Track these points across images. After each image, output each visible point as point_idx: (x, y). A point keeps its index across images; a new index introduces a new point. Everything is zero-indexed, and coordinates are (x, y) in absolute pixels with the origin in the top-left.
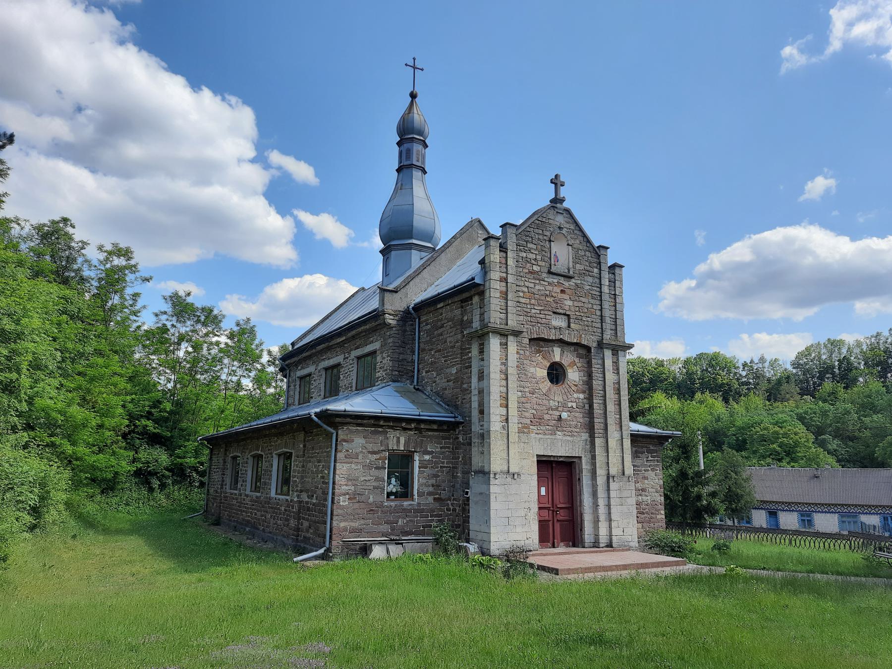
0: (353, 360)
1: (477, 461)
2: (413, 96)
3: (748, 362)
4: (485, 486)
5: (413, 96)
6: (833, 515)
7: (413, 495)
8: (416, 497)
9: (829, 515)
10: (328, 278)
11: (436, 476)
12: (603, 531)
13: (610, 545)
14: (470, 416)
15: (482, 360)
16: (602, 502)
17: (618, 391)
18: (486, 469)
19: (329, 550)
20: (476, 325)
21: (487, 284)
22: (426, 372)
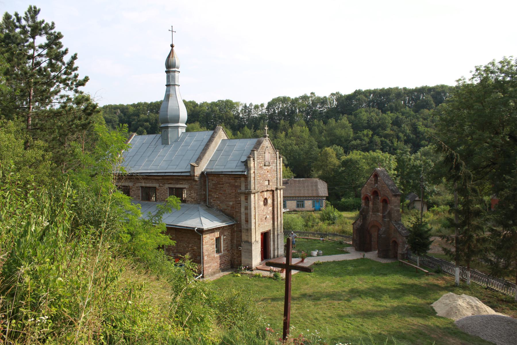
0: (167, 188)
1: (244, 237)
2: (172, 46)
3: (248, 105)
4: (250, 247)
5: (172, 46)
6: (294, 201)
7: (221, 251)
8: (222, 251)
9: (292, 201)
10: (455, 319)
11: (227, 243)
12: (276, 254)
13: (278, 256)
14: (241, 221)
15: (247, 202)
16: (276, 243)
17: (281, 204)
18: (250, 241)
19: (203, 275)
20: (243, 188)
21: (249, 175)
22: (213, 200)
